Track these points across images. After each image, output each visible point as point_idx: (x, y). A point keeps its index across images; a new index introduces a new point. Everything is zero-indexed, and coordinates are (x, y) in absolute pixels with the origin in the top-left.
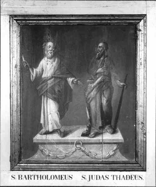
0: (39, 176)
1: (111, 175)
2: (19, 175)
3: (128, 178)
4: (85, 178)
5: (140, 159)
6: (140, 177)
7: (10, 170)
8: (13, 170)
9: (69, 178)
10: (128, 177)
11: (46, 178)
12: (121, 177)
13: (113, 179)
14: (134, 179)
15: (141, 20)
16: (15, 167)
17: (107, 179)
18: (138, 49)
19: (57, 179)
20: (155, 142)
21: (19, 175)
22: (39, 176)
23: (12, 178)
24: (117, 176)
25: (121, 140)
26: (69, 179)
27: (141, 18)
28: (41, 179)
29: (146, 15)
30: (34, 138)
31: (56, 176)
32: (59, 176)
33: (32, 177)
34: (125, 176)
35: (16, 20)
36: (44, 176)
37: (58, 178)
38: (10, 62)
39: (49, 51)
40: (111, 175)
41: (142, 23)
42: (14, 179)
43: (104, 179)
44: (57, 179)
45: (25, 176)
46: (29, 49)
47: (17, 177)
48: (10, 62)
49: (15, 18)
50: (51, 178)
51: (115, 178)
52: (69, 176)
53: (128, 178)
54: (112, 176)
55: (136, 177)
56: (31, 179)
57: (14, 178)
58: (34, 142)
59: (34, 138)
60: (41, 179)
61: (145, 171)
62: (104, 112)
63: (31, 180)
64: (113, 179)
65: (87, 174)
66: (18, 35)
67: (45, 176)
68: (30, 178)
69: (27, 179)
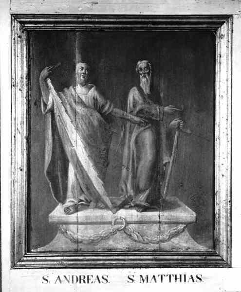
0: (178, 277)
1: (159, 275)
4: (47, 280)
11: (77, 281)
13: (170, 281)
15: (222, 23)
17: (199, 280)
19: (143, 281)
20: (2, 225)
22: (178, 277)
24: (176, 276)
26: (128, 282)
27: (218, 26)
28: (80, 276)
30: (50, 215)
34: (144, 277)
36: (76, 281)
38: (11, 114)
40: (159, 275)
41: (223, 30)
43: (100, 282)
47: (137, 279)
48: (11, 114)
49: (18, 20)
51: (173, 278)
54: (160, 276)
56: (84, 281)
58: (50, 220)
60: (80, 276)
64: (170, 281)
68: (82, 281)
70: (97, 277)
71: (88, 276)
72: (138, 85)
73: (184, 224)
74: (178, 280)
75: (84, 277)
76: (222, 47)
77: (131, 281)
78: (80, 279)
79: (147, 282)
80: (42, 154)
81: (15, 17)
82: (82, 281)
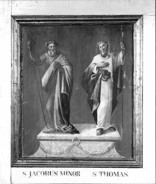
0: (106, 173)
3: (74, 175)
4: (25, 174)
6: (55, 173)
8: (142, 166)
9: (54, 174)
10: (74, 173)
11: (75, 174)
12: (120, 173)
15: (137, 20)
16: (18, 161)
17: (126, 175)
18: (135, 43)
22: (106, 173)
23: (26, 173)
24: (105, 172)
28: (46, 172)
30: (38, 136)
31: (114, 172)
32: (64, 172)
33: (39, 174)
34: (63, 173)
35: (18, 21)
41: (138, 23)
43: (123, 176)
44: (116, 175)
46: (89, 89)
49: (16, 19)
53: (74, 175)
54: (100, 173)
60: (46, 172)
61: (142, 167)
62: (41, 60)
67: (112, 173)
68: (78, 175)
69: (36, 175)
70: (122, 173)
71: (50, 172)
72: (116, 55)
73: (113, 141)
74: (106, 175)
75: (48, 172)
76: (137, 31)
77: (95, 175)
78: (77, 174)
79: (118, 176)
80: (119, 96)
81: (14, 17)
82: (78, 175)
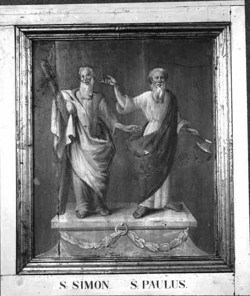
2: (144, 282)
5: (224, 255)
7: (14, 272)
14: (170, 287)
15: (221, 30)
21: (144, 282)
25: (194, 222)
29: (229, 24)
37: (90, 287)
39: (157, 84)
42: (183, 286)
45: (152, 282)
50: (173, 285)
52: (180, 283)
55: (175, 283)
57: (136, 286)
59: (55, 219)
63: (81, 290)
65: (139, 278)
66: (218, 71)
